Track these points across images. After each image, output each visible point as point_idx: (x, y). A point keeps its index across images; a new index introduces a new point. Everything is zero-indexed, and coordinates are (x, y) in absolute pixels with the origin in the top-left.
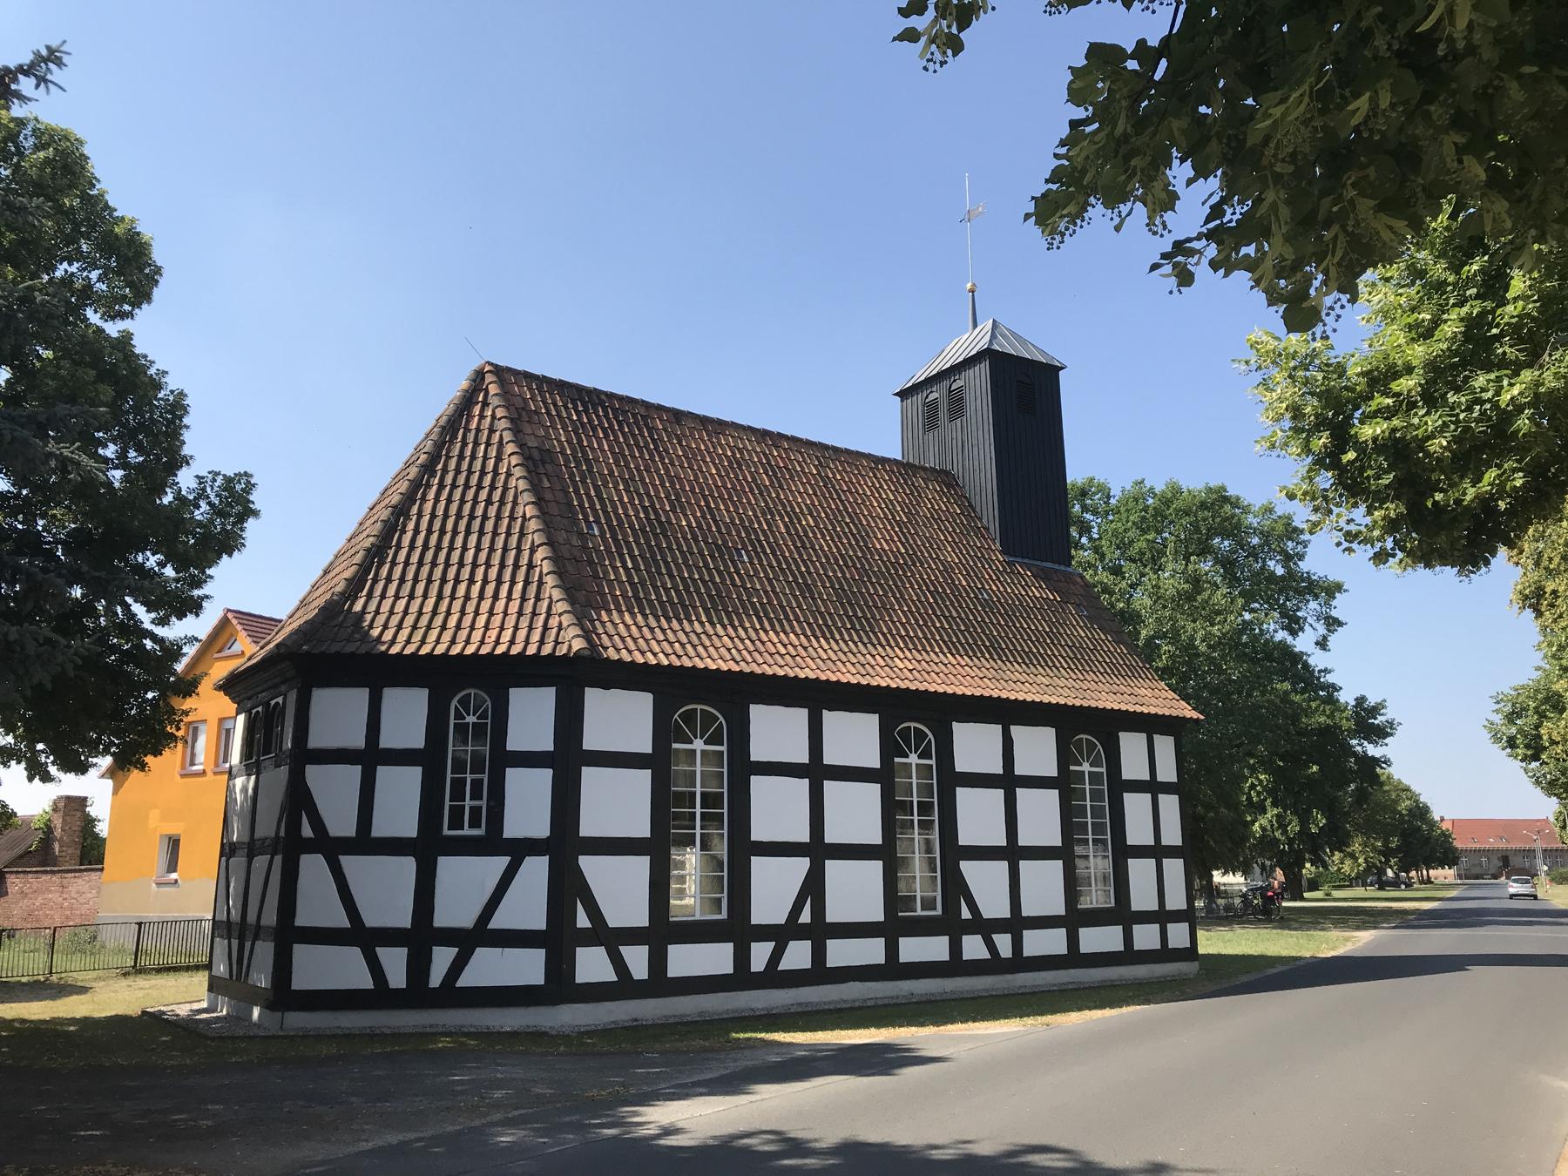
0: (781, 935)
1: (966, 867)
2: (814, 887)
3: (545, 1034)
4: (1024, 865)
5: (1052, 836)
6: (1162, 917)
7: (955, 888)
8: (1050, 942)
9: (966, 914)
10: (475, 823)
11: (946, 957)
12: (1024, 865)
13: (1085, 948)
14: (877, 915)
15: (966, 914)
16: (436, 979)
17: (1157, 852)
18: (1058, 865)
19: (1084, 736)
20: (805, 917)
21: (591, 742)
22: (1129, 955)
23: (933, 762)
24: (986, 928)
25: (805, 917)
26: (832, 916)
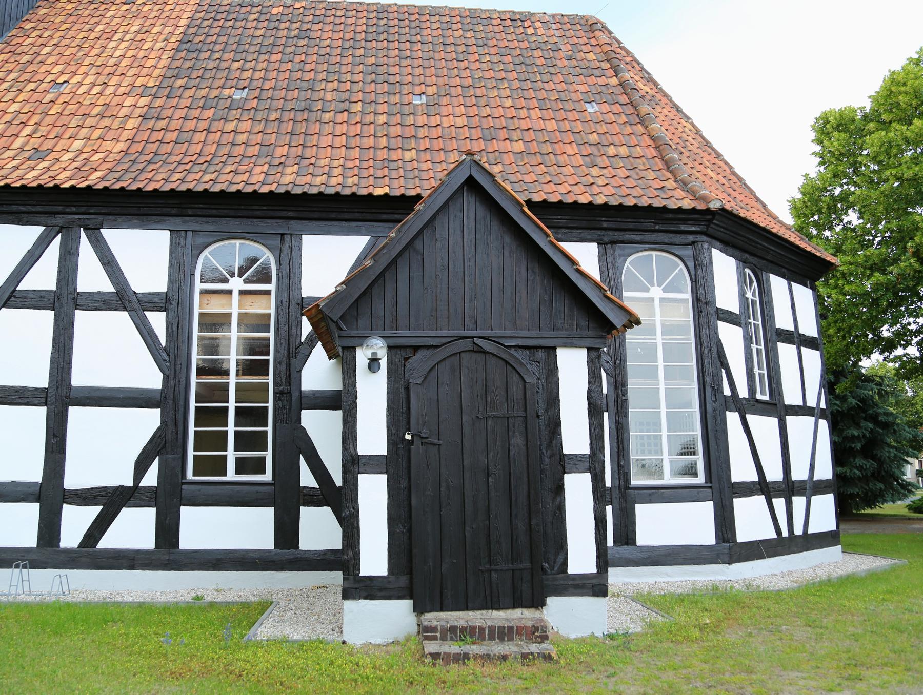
9: (307, 479)
15: (307, 479)
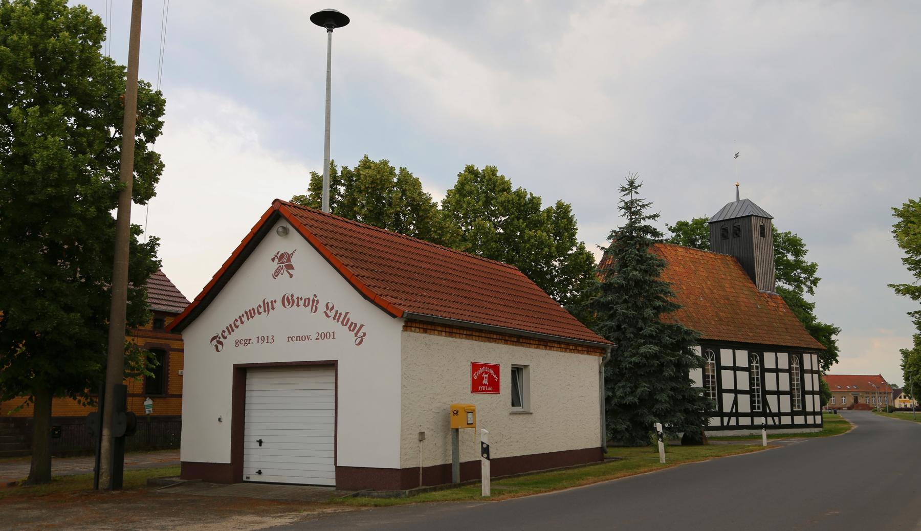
0: (730, 415)
1: (768, 397)
2: (735, 402)
3: (740, 436)
4: (733, 388)
5: (724, 373)
6: (814, 414)
7: (765, 403)
8: (786, 420)
9: (768, 411)
10: (799, 407)
11: (720, 425)
12: (733, 388)
13: (740, 424)
14: (749, 411)
15: (768, 411)
16: (725, 424)
17: (813, 393)
18: (789, 396)
19: (754, 354)
20: (734, 411)
21: (781, 396)
22: (806, 426)
23: (714, 362)
24: (772, 415)
25: (734, 411)
26: (740, 411)
